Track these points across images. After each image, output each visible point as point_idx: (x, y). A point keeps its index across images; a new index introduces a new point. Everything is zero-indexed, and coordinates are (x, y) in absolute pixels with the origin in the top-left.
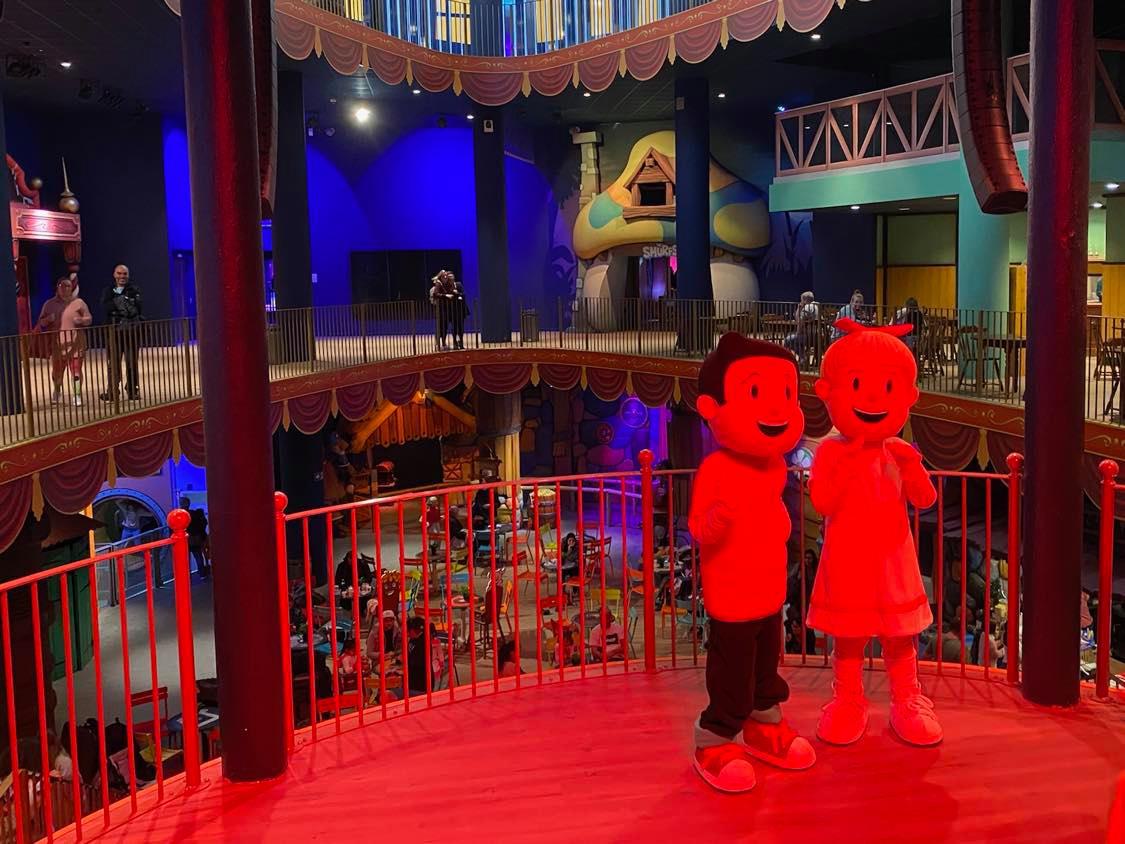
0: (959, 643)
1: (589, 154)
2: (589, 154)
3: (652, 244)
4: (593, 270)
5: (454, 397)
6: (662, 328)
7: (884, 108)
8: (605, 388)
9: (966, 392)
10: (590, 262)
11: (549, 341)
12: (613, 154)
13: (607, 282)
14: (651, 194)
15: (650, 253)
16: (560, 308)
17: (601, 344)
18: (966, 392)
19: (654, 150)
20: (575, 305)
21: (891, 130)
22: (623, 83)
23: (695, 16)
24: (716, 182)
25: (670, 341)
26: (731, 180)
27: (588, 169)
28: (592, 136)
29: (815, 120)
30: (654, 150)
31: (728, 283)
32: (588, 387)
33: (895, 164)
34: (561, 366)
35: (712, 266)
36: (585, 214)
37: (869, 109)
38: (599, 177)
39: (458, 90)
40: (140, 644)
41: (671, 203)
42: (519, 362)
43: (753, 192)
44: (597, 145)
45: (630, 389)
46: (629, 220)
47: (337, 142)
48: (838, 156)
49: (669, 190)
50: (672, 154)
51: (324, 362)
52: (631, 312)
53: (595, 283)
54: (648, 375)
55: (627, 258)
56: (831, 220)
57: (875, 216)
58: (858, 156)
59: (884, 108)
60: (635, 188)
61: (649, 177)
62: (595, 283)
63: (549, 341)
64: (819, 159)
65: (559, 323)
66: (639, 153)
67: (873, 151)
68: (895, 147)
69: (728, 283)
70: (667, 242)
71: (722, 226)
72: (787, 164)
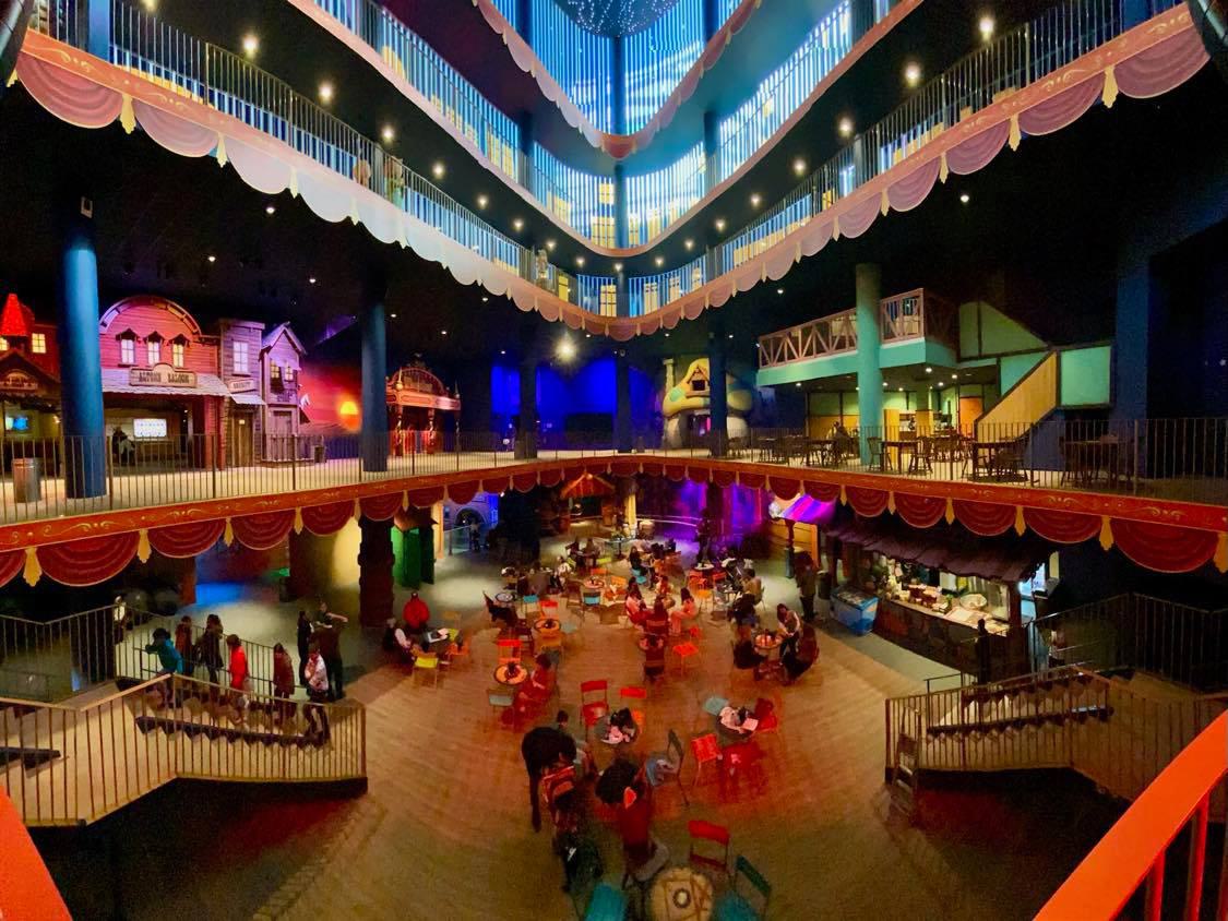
0: (787, 531)
1: (670, 369)
2: (670, 369)
3: (699, 408)
4: (671, 422)
5: (605, 476)
6: (703, 447)
7: (815, 330)
8: (917, 514)
9: (874, 472)
10: (670, 418)
11: (648, 453)
12: (680, 368)
13: (1162, 865)
14: (698, 385)
15: (697, 413)
16: (657, 440)
17: (671, 454)
18: (874, 472)
19: (701, 366)
20: (663, 437)
21: (818, 343)
22: (684, 322)
23: (719, 281)
24: (729, 380)
25: (706, 453)
26: (734, 380)
27: (670, 375)
28: (671, 361)
29: (778, 342)
30: (701, 366)
31: (734, 426)
32: (847, 503)
33: (822, 358)
34: (654, 465)
35: (728, 419)
36: (667, 398)
37: (806, 333)
38: (675, 380)
39: (607, 333)
40: (58, 730)
41: (708, 389)
42: (634, 463)
43: (746, 385)
44: (674, 365)
45: (687, 474)
46: (688, 397)
47: (549, 368)
48: (791, 357)
49: (706, 383)
50: (708, 368)
51: (540, 459)
52: (689, 440)
53: (672, 427)
54: (698, 471)
55: (687, 415)
56: (784, 390)
57: (813, 386)
58: (802, 355)
59: (815, 330)
60: (691, 383)
61: (698, 377)
62: (672, 427)
63: (648, 453)
64: (781, 359)
65: (658, 447)
66: (693, 367)
67: (809, 354)
68: (820, 350)
69: (734, 426)
70: (705, 407)
71: (732, 400)
72: (765, 363)
